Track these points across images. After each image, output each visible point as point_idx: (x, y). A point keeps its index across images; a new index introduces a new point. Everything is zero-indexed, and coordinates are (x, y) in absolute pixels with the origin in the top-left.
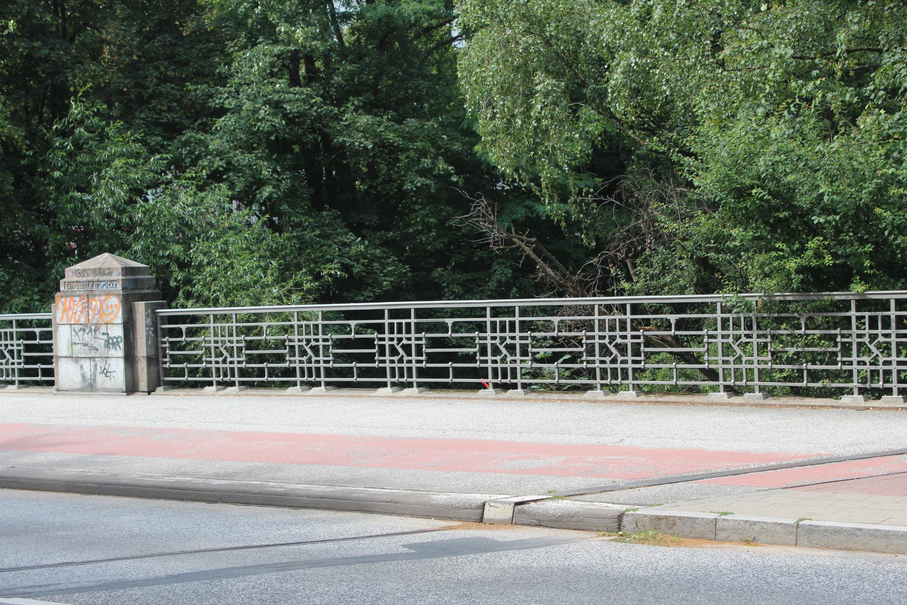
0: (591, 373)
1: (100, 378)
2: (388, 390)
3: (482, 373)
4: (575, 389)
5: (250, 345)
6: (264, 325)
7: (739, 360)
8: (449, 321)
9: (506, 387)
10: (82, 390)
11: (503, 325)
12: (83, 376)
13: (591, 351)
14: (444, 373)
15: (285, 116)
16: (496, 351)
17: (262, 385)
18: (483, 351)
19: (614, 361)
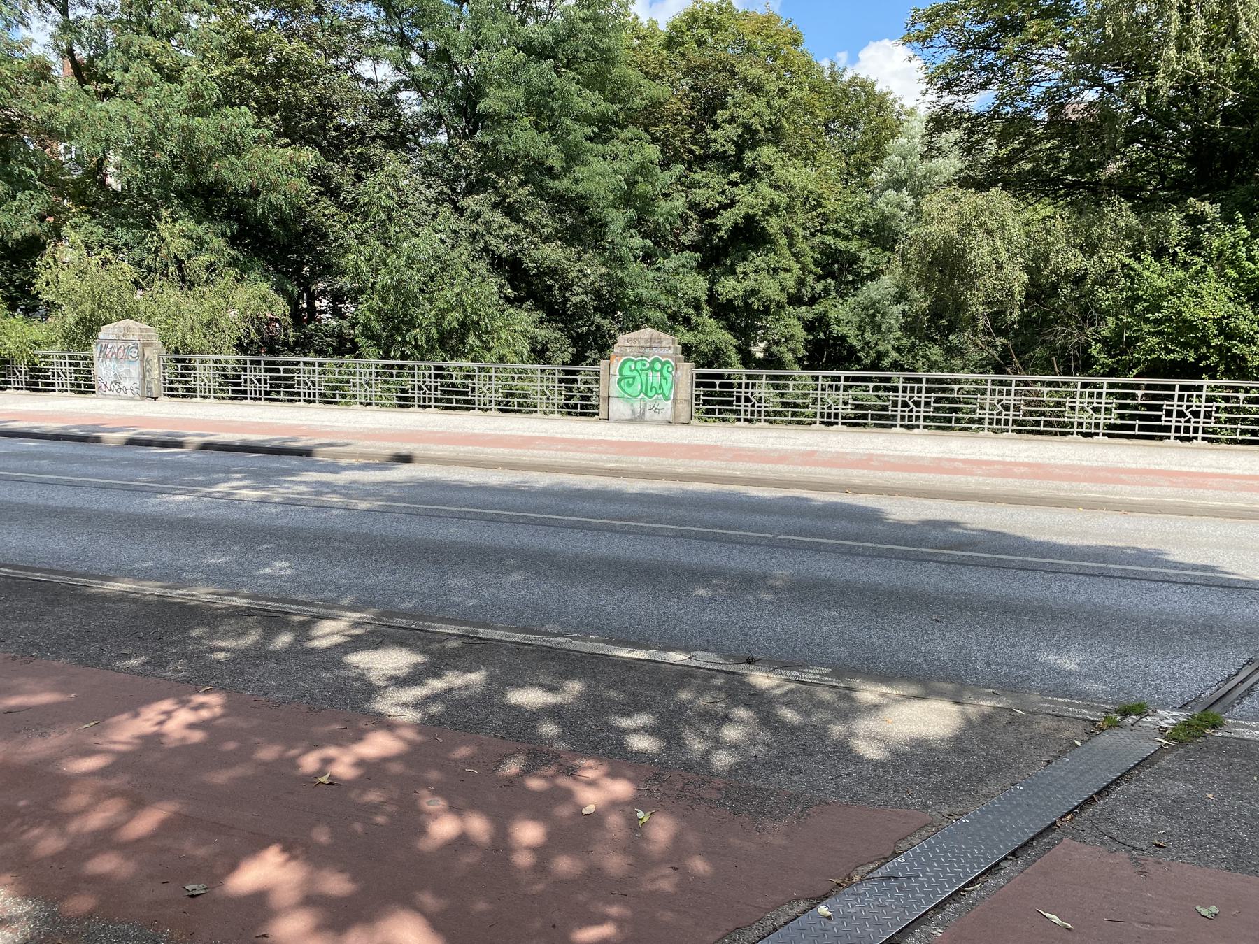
0: (299, 394)
1: (648, 414)
2: (56, 393)
3: (1168, 429)
4: (291, 401)
5: (272, 378)
6: (579, 378)
7: (911, 411)
8: (282, 368)
9: (910, 427)
10: (631, 421)
11: (912, 389)
12: (633, 411)
13: (927, 404)
14: (1132, 427)
15: (689, 248)
16: (420, 388)
17: (1040, 433)
18: (739, 399)
19: (1188, 421)
